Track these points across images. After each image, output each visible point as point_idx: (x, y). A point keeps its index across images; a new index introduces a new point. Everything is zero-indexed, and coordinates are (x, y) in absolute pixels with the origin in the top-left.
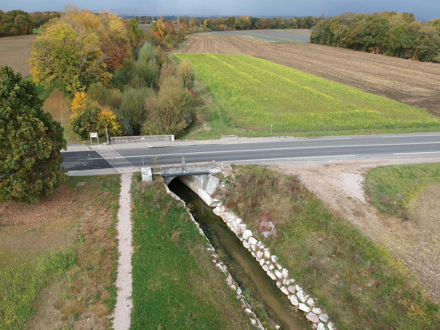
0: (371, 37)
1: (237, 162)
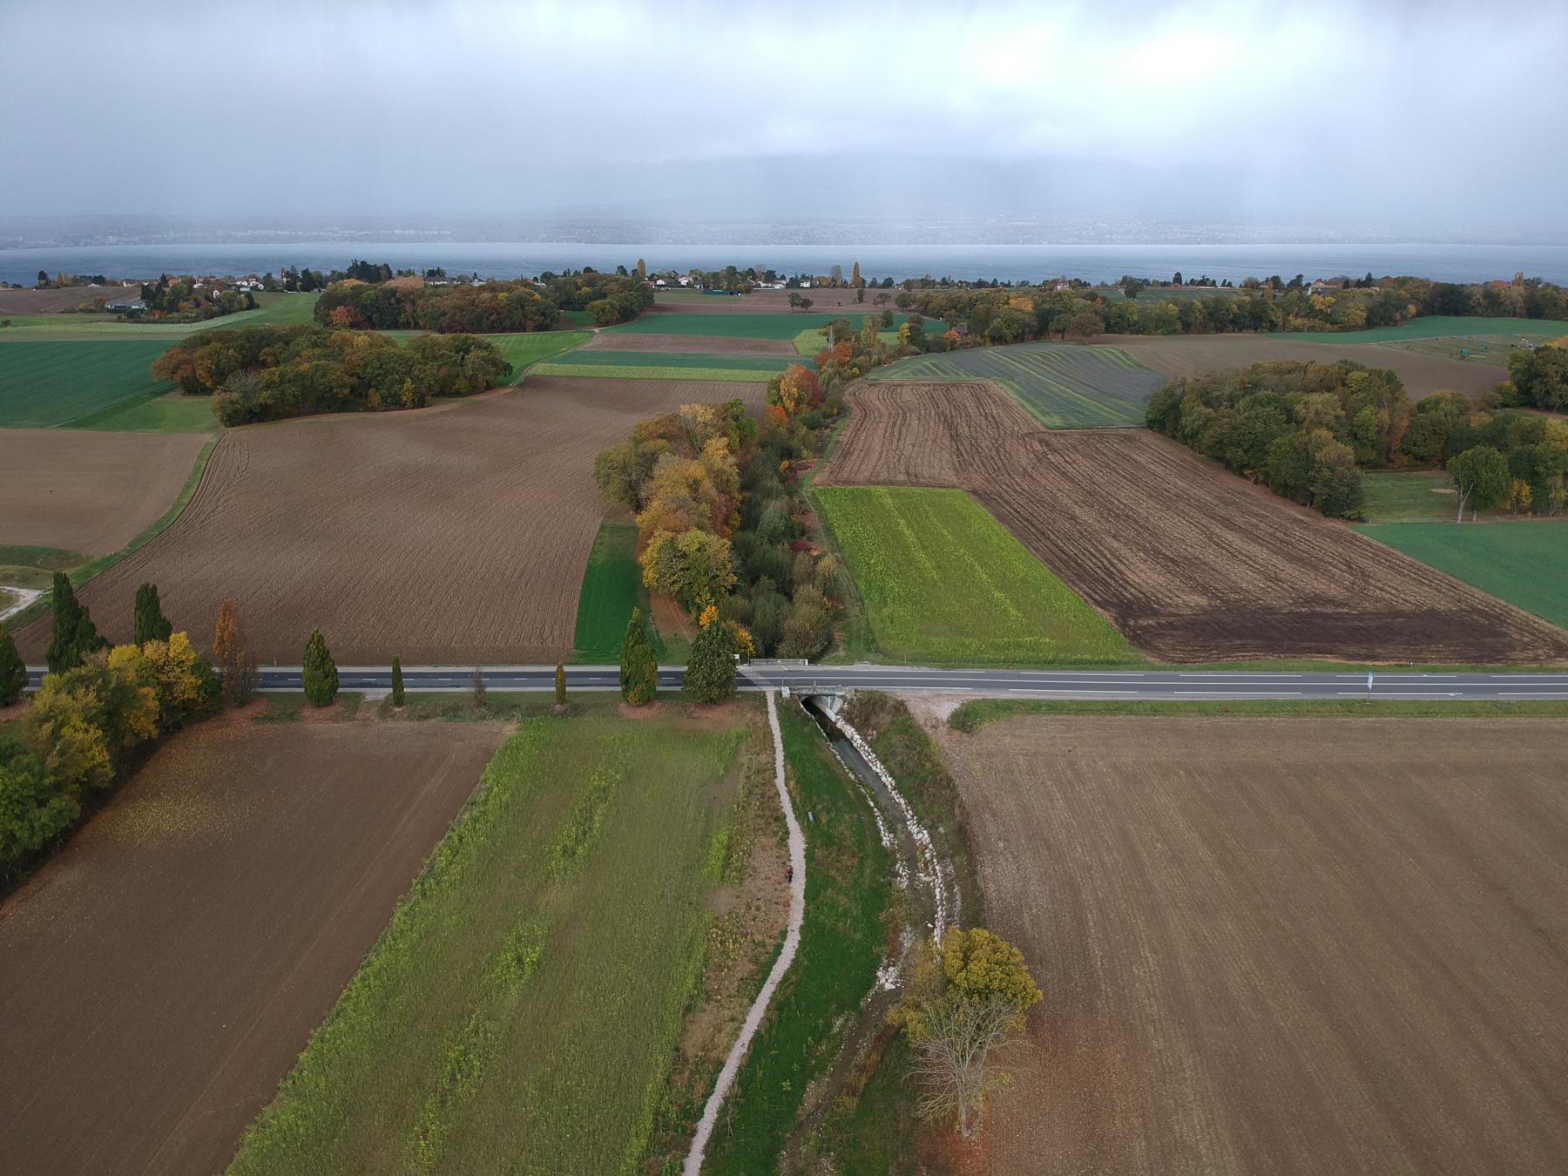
0: (1240, 452)
1: (860, 688)
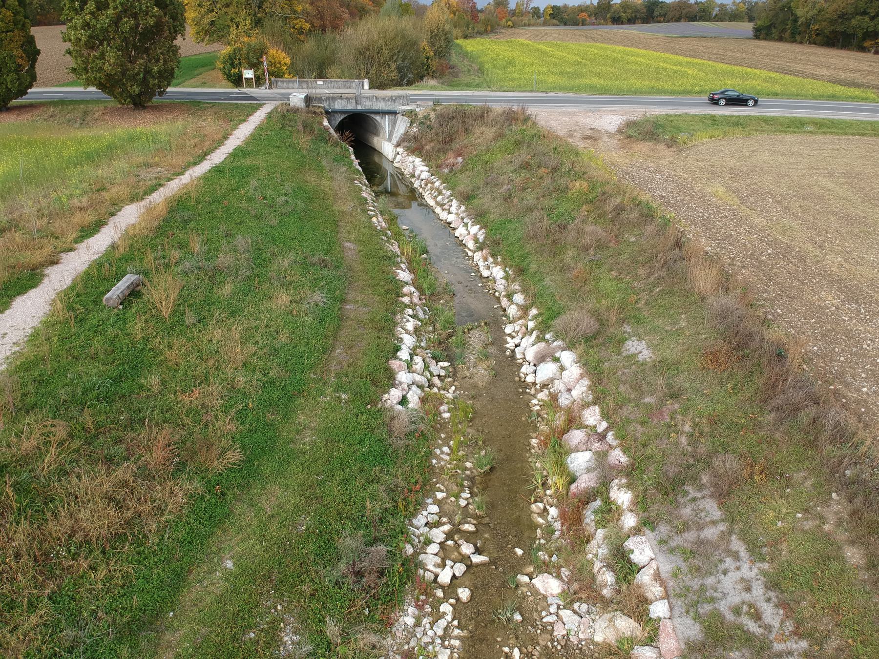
0: (867, 19)
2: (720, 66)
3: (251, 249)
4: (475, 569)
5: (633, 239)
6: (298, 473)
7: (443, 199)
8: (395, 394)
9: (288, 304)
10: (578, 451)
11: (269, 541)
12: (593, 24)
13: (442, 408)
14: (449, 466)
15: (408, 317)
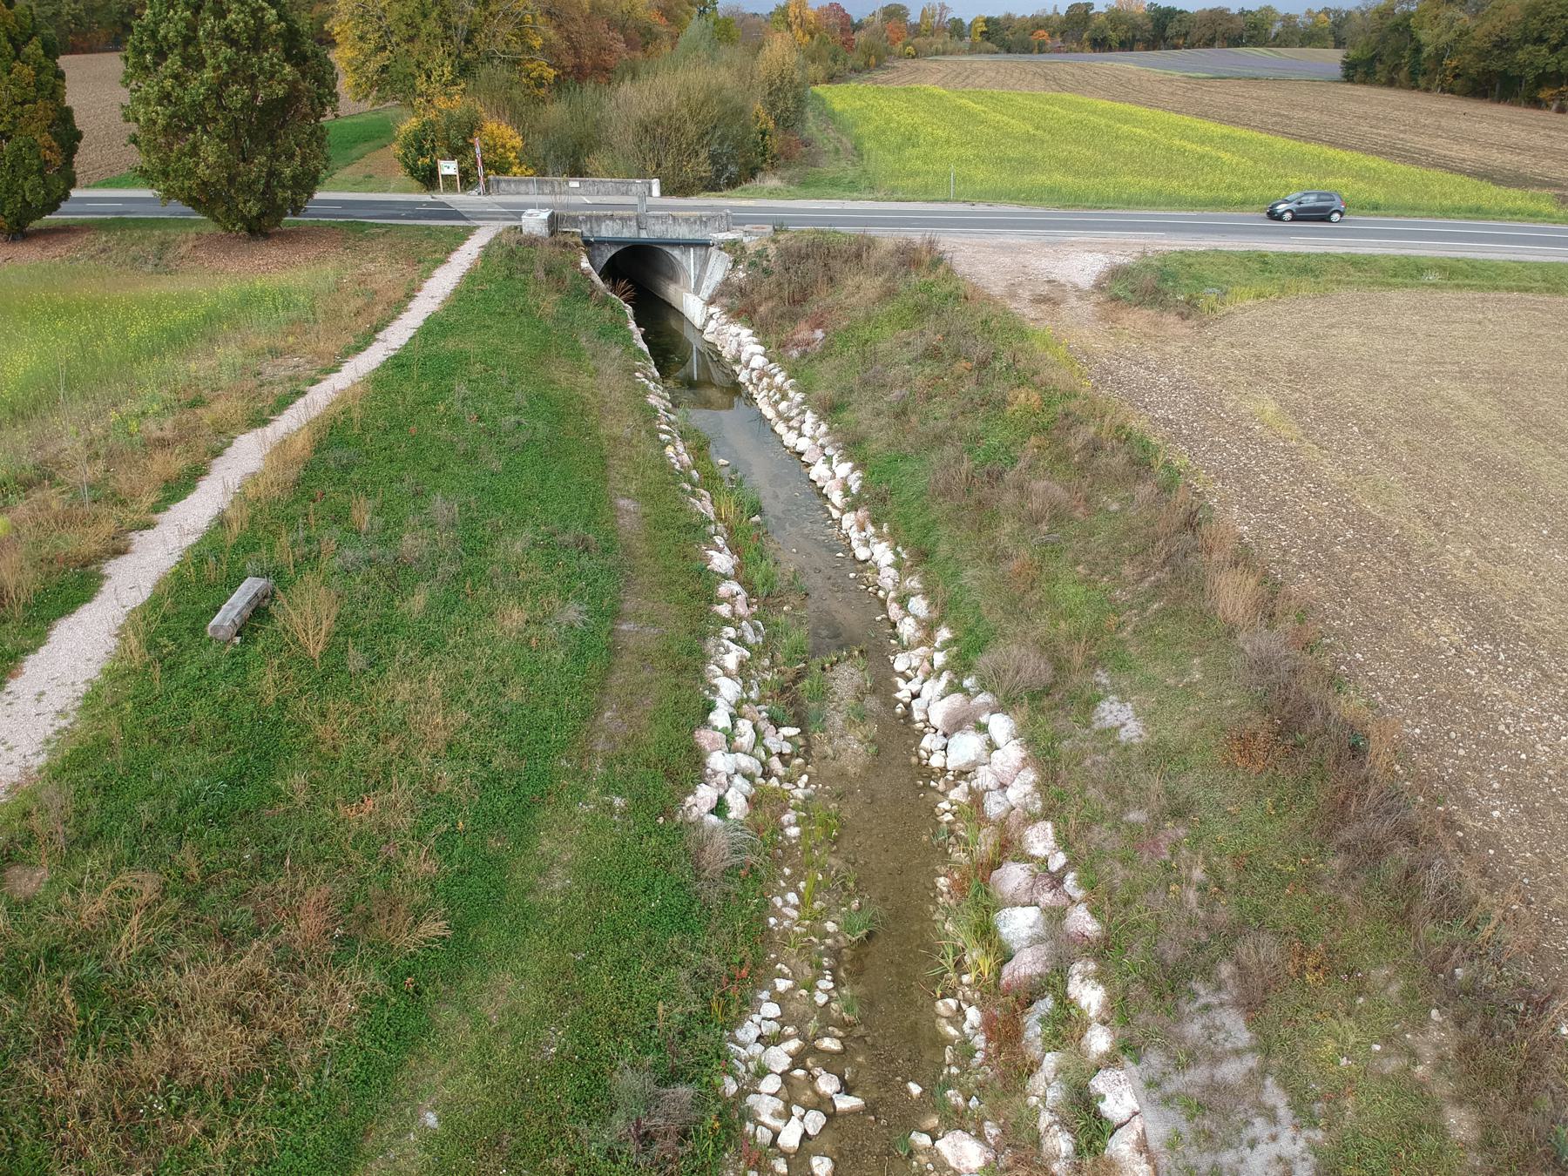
0: (1544, 50)
2: (1281, 144)
3: (458, 522)
4: (840, 1121)
5: (1115, 507)
6: (543, 949)
7: (789, 408)
8: (705, 795)
9: (522, 626)
10: (1015, 905)
11: (496, 1076)
12: (1058, 50)
13: (785, 818)
14: (797, 929)
15: (727, 642)
